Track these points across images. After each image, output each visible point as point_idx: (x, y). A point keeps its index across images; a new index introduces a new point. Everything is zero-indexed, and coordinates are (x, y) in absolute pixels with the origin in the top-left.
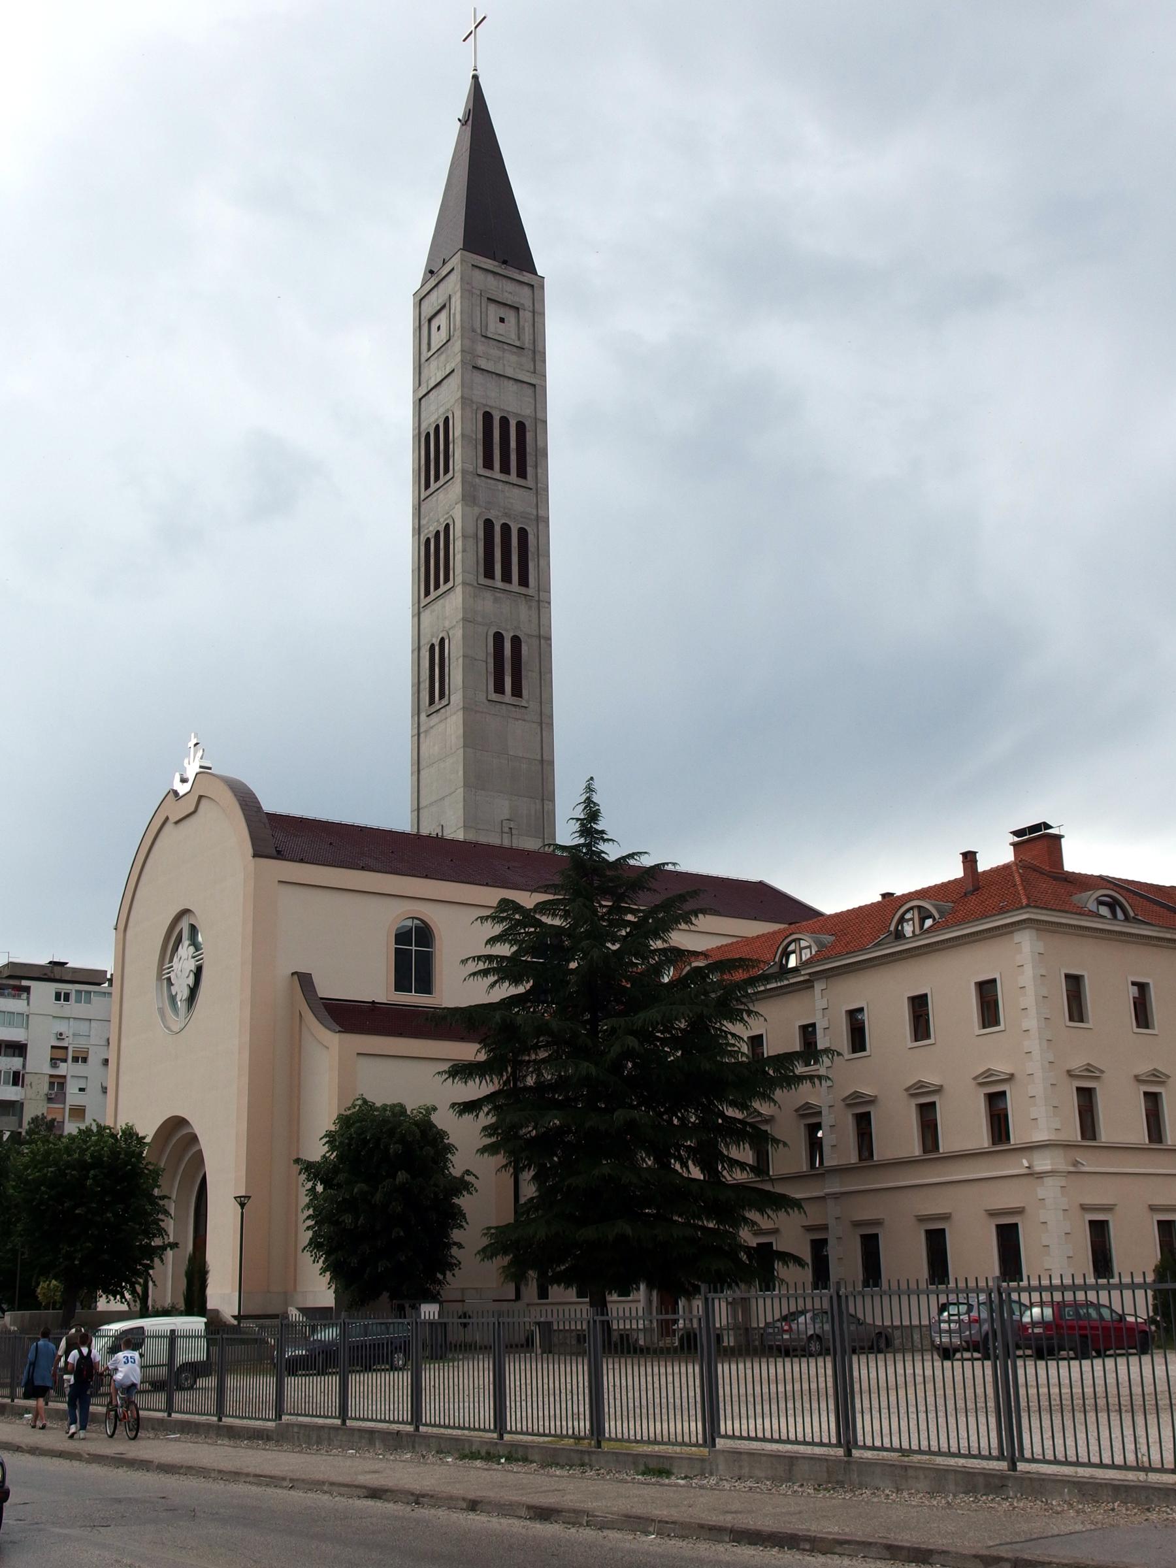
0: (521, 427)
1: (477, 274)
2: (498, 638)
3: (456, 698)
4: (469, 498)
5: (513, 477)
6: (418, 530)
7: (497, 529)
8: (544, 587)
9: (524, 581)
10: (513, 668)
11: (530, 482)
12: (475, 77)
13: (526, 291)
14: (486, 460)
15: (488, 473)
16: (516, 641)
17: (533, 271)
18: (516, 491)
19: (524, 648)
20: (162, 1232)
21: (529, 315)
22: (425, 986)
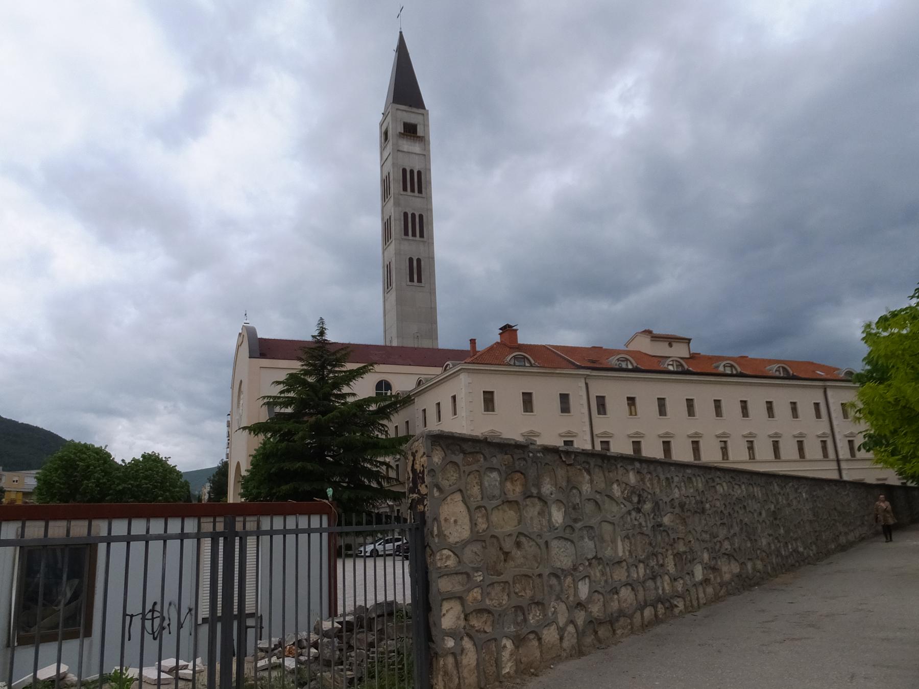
1: (399, 112)
2: (411, 260)
3: (394, 285)
4: (397, 204)
6: (383, 219)
7: (410, 216)
8: (431, 237)
9: (422, 236)
10: (417, 271)
11: (424, 194)
12: (401, 33)
13: (421, 117)
16: (419, 261)
18: (418, 200)
19: (422, 263)
21: (422, 127)
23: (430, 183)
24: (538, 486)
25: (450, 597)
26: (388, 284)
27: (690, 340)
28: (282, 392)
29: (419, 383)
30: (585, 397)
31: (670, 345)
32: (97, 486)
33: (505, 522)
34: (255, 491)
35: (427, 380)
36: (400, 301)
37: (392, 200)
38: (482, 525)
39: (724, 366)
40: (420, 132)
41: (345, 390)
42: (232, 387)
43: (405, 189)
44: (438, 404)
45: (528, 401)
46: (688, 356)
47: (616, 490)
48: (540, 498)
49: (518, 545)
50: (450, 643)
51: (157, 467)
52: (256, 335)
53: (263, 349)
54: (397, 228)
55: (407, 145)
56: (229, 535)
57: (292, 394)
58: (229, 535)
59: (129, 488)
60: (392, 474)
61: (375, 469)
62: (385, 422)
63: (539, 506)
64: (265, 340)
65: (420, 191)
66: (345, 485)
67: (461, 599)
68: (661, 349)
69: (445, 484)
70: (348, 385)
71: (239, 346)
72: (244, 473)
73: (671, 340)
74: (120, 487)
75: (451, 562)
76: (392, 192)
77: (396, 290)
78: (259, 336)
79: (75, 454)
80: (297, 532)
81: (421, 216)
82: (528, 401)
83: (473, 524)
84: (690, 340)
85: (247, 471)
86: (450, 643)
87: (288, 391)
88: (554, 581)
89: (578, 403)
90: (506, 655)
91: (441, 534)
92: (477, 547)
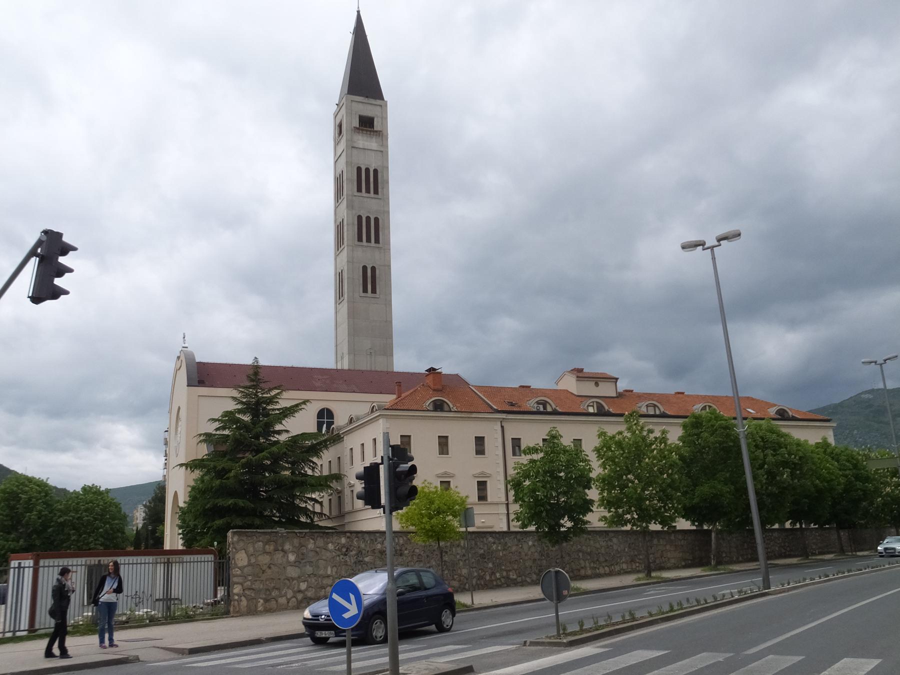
0: (376, 171)
2: (365, 268)
3: (346, 296)
4: (350, 206)
5: (372, 194)
9: (377, 241)
11: (380, 196)
12: (358, 12)
13: (379, 108)
14: (364, 184)
15: (359, 194)
16: (373, 269)
17: (382, 99)
18: (374, 200)
20: (319, 457)
21: (380, 120)
22: (91, 570)
23: (388, 182)
24: (283, 546)
25: (237, 583)
26: (340, 294)
27: (617, 379)
28: (217, 429)
29: (351, 421)
30: (500, 440)
31: (597, 384)
32: (39, 518)
33: (264, 560)
34: (192, 524)
35: (358, 419)
36: (352, 314)
37: (345, 202)
38: (253, 560)
39: (647, 406)
40: (377, 126)
41: (278, 427)
42: (170, 412)
43: (359, 190)
44: (363, 445)
45: (443, 444)
46: (615, 395)
47: (330, 546)
48: (283, 550)
49: (270, 568)
50: (236, 597)
51: (97, 500)
52: (194, 359)
53: (203, 375)
54: (350, 233)
55: (362, 141)
56: (168, 563)
57: (227, 432)
58: (168, 563)
59: (70, 521)
60: (318, 508)
61: (304, 505)
62: (315, 459)
63: (282, 554)
64: (204, 364)
65: (376, 192)
66: (277, 519)
67: (242, 584)
68: (589, 389)
69: (238, 547)
70: (281, 423)
71: (177, 370)
72: (181, 504)
73: (598, 379)
74: (62, 519)
75: (239, 572)
76: (345, 193)
77: (348, 302)
78: (198, 360)
79: (17, 486)
80: (49, 566)
81: (377, 220)
82: (443, 444)
83: (249, 560)
84: (617, 379)
85: (185, 502)
86: (236, 597)
87: (224, 428)
88: (287, 582)
89: (493, 445)
90: (260, 604)
91: (235, 563)
92: (250, 568)
